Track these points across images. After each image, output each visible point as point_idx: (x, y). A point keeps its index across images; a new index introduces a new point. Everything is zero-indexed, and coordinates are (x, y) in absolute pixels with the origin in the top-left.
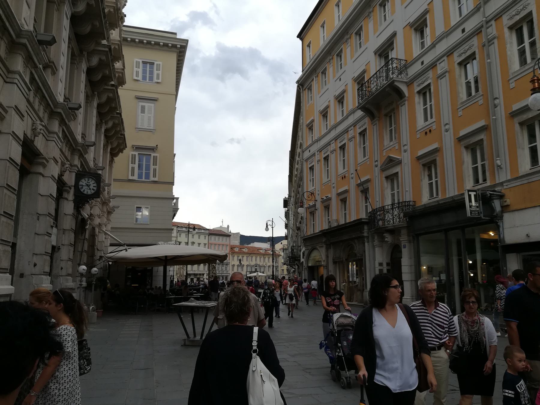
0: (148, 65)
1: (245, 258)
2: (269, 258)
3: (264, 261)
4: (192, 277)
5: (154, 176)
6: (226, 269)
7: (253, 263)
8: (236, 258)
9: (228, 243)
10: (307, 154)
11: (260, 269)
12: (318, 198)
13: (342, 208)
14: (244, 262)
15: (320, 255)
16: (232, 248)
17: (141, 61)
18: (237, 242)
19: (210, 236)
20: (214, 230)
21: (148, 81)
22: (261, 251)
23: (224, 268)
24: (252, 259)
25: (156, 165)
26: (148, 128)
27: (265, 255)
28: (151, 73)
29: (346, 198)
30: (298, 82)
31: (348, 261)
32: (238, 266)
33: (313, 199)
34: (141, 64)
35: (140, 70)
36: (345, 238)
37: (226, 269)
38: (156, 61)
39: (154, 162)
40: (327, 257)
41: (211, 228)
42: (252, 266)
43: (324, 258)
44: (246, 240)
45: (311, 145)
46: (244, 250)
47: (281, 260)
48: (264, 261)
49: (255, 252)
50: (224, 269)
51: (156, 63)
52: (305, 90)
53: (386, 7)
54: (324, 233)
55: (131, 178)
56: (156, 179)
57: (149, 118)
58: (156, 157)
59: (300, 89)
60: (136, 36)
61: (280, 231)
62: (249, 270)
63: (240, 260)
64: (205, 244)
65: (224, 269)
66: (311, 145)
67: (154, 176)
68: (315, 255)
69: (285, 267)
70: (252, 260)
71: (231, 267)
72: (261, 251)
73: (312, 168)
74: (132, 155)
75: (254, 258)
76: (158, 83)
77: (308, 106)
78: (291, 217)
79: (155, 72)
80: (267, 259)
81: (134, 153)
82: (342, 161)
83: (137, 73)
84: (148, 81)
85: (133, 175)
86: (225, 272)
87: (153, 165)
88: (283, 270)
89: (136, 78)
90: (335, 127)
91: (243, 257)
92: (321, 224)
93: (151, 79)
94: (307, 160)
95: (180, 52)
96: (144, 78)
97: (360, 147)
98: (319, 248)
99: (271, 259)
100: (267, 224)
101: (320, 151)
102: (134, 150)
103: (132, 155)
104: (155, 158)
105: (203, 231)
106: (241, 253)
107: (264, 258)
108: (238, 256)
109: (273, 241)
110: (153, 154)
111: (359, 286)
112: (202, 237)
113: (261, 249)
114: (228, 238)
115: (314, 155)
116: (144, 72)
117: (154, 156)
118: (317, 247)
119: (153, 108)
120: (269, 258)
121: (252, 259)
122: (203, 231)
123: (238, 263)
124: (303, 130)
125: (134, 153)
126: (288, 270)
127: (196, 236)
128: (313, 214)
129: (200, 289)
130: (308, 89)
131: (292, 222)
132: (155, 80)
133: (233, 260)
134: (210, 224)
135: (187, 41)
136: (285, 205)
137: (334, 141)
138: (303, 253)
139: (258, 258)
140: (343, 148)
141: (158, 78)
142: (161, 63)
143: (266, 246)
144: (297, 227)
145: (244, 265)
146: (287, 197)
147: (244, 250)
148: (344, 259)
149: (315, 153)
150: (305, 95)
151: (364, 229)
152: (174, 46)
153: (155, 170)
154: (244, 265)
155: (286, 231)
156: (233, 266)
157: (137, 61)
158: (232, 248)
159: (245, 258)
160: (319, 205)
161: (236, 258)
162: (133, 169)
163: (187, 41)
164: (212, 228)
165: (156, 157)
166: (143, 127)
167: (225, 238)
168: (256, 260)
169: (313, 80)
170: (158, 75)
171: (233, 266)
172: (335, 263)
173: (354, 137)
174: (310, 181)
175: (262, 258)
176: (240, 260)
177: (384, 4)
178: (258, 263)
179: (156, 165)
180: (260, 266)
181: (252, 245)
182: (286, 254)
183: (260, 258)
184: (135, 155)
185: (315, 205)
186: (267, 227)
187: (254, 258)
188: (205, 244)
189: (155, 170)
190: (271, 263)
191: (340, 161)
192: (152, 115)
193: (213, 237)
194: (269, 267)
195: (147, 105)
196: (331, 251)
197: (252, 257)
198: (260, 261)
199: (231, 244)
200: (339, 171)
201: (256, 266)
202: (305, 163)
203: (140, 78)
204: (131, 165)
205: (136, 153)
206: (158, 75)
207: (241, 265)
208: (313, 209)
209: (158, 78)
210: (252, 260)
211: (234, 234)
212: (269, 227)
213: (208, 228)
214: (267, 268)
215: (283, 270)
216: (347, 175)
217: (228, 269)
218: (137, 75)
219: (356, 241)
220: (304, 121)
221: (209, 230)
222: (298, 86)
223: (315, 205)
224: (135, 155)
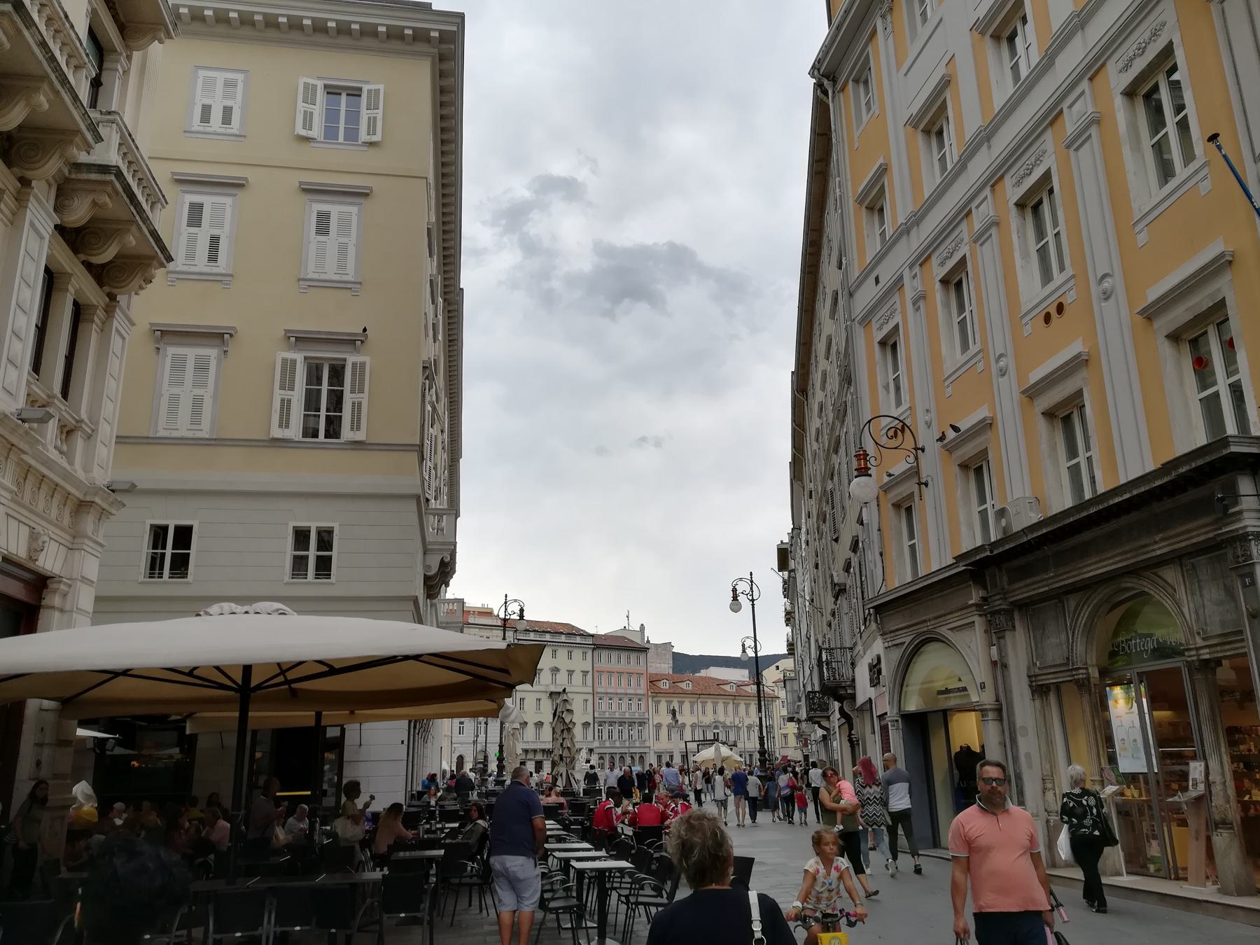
0: (344, 97)
1: (686, 706)
2: (748, 706)
3: (736, 712)
4: (539, 757)
5: (356, 426)
6: (640, 737)
7: (708, 719)
8: (663, 706)
9: (641, 668)
10: (867, 294)
11: (727, 734)
12: (926, 437)
13: (1053, 448)
14: (686, 718)
15: (962, 660)
16: (653, 681)
17: (320, 84)
18: (665, 667)
19: (596, 653)
20: (606, 636)
21: (341, 139)
22: (727, 688)
23: (634, 733)
24: (703, 707)
25: (361, 391)
26: (337, 278)
27: (736, 696)
28: (353, 117)
29: (1079, 393)
30: (815, 70)
31: (1110, 676)
32: (669, 726)
33: (909, 444)
34: (320, 94)
35: (318, 110)
36: (1094, 568)
37: (640, 737)
38: (367, 82)
39: (353, 381)
40: (999, 666)
41: (602, 630)
42: (704, 728)
43: (981, 672)
44: (686, 664)
45: (879, 258)
46: (683, 685)
47: (780, 710)
48: (736, 712)
49: (714, 691)
50: (635, 737)
51: (366, 88)
52: (843, 90)
53: (1019, 40)
54: (981, 568)
55: (277, 433)
56: (360, 436)
57: (343, 250)
58: (363, 365)
59: (825, 93)
60: (304, 9)
61: (774, 640)
62: (699, 736)
63: (674, 713)
64: (585, 673)
65: (635, 737)
66: (879, 258)
67: (356, 426)
68: (935, 669)
69: (792, 728)
70: (704, 713)
71: (652, 731)
72: (727, 688)
73: (889, 344)
74: (284, 361)
75: (709, 706)
76: (371, 144)
77: (856, 134)
78: (804, 584)
79: (365, 114)
80: (742, 708)
81: (290, 355)
82: (1035, 258)
83: (308, 118)
84: (341, 139)
85: (285, 422)
86: (637, 744)
87: (352, 392)
88: (785, 736)
89: (303, 133)
90: (988, 138)
91: (681, 703)
92: (951, 530)
93: (352, 135)
94: (866, 320)
95: (442, 58)
96: (331, 133)
97: (1137, 148)
98: (949, 635)
99: (753, 708)
100: (743, 645)
101: (923, 260)
102: (290, 348)
103: (284, 361)
104: (359, 369)
105: (578, 640)
106: (675, 693)
107: (736, 706)
108: (669, 703)
109: (757, 665)
110: (351, 359)
111: (1217, 800)
112: (577, 653)
113: (726, 683)
114: (642, 656)
115: (898, 284)
116: (331, 116)
117: (354, 365)
118: (944, 631)
119: (354, 219)
120: (748, 706)
121: (703, 707)
122: (578, 640)
123: (668, 719)
124: (845, 217)
125: (290, 355)
126: (800, 736)
127: (563, 653)
128: (905, 508)
129: (473, 821)
130: (856, 81)
131: (804, 604)
132: (363, 136)
133: (657, 711)
134: (600, 624)
135: (461, 16)
136: (783, 563)
137: (987, 191)
138: (875, 669)
139: (720, 707)
140: (1031, 205)
141: (371, 130)
142: (381, 87)
143: (742, 675)
144: (834, 585)
145: (684, 725)
146: (786, 540)
147: (683, 685)
148: (1094, 673)
149: (901, 278)
150: (844, 107)
151: (1235, 497)
152: (420, 36)
153: (357, 407)
154: (684, 725)
155: (789, 629)
156: (658, 726)
157: (306, 85)
158: (653, 681)
159: (686, 706)
160: (932, 464)
161: (663, 706)
162: (286, 405)
163: (461, 16)
164: (602, 632)
165: (363, 365)
166: (323, 277)
167: (633, 656)
168: (715, 712)
169: (874, 32)
170: (372, 122)
171: (658, 726)
172: (1040, 690)
173: (1096, 121)
174: (887, 387)
175: (730, 707)
176: (674, 713)
177: (1007, 32)
178: (722, 719)
179: (361, 391)
180: (725, 726)
181: (703, 673)
182: (793, 691)
183: (726, 705)
184: (294, 362)
185: (915, 472)
186: (735, 598)
187: (709, 706)
188: (585, 673)
189: (357, 407)
190: (753, 718)
191: (1026, 256)
192: (351, 241)
193: (605, 654)
194: (749, 727)
195: (336, 210)
196: (1018, 647)
197: (704, 703)
198: (726, 713)
199: (651, 670)
200: (1023, 298)
201: (716, 727)
202: (859, 332)
203: (317, 132)
204: (278, 394)
205: (299, 357)
206: (372, 122)
207: (676, 725)
208: (911, 486)
209: (371, 130)
210: (704, 713)
211: (656, 645)
212: (742, 598)
213: (592, 632)
214: (744, 733)
215: (785, 736)
216: (1067, 300)
217: (645, 735)
218: (308, 124)
219: (1171, 574)
220: (848, 182)
221: (593, 636)
222: (819, 86)
223: (915, 472)
224: (294, 362)
